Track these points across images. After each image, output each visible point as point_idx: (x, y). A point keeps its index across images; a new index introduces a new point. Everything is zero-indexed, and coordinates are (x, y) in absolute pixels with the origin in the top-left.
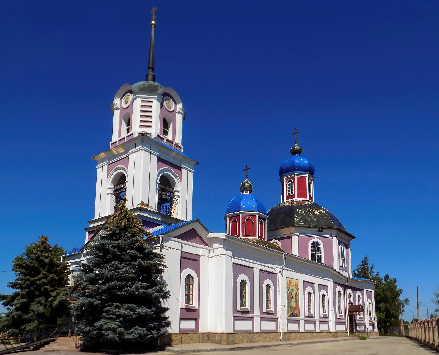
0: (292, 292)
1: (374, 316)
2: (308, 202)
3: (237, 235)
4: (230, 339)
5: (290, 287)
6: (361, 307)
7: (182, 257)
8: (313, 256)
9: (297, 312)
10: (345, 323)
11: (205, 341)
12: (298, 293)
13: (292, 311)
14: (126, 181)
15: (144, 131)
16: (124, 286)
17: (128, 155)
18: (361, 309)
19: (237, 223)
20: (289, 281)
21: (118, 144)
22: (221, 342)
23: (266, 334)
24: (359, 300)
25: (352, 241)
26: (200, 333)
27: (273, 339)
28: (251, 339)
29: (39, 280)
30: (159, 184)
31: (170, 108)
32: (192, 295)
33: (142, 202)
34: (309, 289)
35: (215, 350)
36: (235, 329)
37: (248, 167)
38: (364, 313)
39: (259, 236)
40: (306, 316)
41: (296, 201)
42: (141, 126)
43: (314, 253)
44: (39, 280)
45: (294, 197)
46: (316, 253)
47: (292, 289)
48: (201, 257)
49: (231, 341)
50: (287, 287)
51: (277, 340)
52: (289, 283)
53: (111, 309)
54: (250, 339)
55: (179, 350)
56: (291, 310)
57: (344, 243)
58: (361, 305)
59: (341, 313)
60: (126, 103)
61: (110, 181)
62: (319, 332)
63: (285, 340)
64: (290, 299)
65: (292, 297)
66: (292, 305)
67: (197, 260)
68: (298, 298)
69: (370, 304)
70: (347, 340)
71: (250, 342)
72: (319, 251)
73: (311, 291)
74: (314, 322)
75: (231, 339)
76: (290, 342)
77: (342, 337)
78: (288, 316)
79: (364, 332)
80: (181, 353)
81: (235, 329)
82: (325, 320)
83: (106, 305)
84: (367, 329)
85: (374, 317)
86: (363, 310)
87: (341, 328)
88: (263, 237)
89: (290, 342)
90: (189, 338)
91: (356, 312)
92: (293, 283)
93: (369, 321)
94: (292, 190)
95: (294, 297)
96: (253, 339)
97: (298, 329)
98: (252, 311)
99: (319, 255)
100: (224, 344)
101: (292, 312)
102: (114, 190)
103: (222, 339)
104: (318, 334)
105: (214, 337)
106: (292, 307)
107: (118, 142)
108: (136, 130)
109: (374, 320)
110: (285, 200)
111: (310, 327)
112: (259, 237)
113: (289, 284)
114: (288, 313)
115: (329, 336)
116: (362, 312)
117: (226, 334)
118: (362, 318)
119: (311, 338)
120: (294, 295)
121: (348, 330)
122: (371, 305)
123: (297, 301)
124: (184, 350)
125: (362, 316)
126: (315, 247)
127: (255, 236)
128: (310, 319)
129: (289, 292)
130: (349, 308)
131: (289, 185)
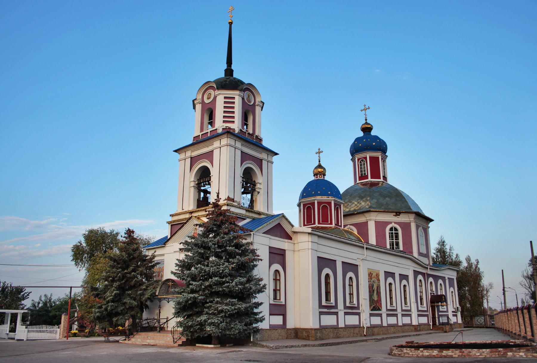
0: (373, 285)
1: (457, 306)
2: (383, 183)
3: (313, 223)
4: (317, 335)
5: (371, 279)
6: (443, 297)
7: (270, 252)
8: (391, 243)
9: (379, 305)
10: (428, 315)
11: (293, 337)
12: (380, 285)
13: (374, 305)
14: (210, 176)
15: (227, 127)
16: (224, 283)
17: (213, 150)
18: (443, 299)
19: (312, 210)
20: (371, 273)
21: (201, 138)
22: (309, 338)
23: (350, 329)
24: (441, 289)
25: (431, 224)
26: (287, 329)
27: (357, 334)
28: (337, 335)
29: (130, 273)
30: (242, 177)
31: (250, 102)
32: (280, 290)
33: (228, 197)
34: (390, 280)
35: (306, 346)
36: (322, 324)
37: (320, 150)
38: (446, 303)
39: (336, 223)
40: (388, 309)
41: (370, 182)
42: (224, 122)
43: (392, 240)
44: (130, 273)
45: (368, 178)
46: (394, 239)
47: (373, 281)
48: (287, 252)
49: (318, 337)
50: (369, 279)
51: (361, 336)
52: (370, 275)
53: (213, 305)
54: (336, 334)
55: (273, 346)
56: (373, 303)
57: (422, 227)
58: (444, 295)
59: (423, 305)
60: (208, 98)
61: (193, 174)
62: (401, 326)
63: (370, 335)
64: (372, 292)
65: (374, 289)
66: (374, 298)
67: (283, 255)
68: (380, 290)
69: (452, 292)
70: (430, 333)
71: (335, 338)
72: (397, 237)
73: (392, 282)
74: (396, 315)
75: (319, 335)
76: (374, 337)
77: (424, 330)
78: (371, 309)
79: (448, 323)
80: (275, 349)
81: (322, 324)
82: (407, 313)
83: (208, 301)
84: (451, 320)
85: (458, 307)
86: (446, 301)
87: (424, 320)
88: (340, 225)
89: (374, 337)
90: (278, 334)
91: (438, 302)
92: (374, 274)
93: (453, 312)
94: (365, 171)
95: (376, 289)
96: (338, 334)
97: (380, 323)
98: (336, 307)
99: (397, 242)
100: (312, 340)
101: (374, 306)
102: (197, 183)
103: (309, 335)
104: (400, 327)
105: (302, 333)
106: (374, 300)
107: (201, 136)
108: (219, 124)
109: (458, 310)
110: (358, 182)
111: (392, 320)
112: (335, 225)
113: (370, 275)
114: (370, 307)
115: (412, 330)
116: (444, 303)
117: (314, 330)
118: (203, 131)
119: (394, 333)
120: (375, 287)
121: (431, 323)
122: (454, 293)
123: (379, 293)
124: (278, 346)
125: (445, 307)
126: (393, 233)
127: (331, 223)
128: (392, 313)
129: (371, 284)
130: (431, 298)
131: (361, 165)
